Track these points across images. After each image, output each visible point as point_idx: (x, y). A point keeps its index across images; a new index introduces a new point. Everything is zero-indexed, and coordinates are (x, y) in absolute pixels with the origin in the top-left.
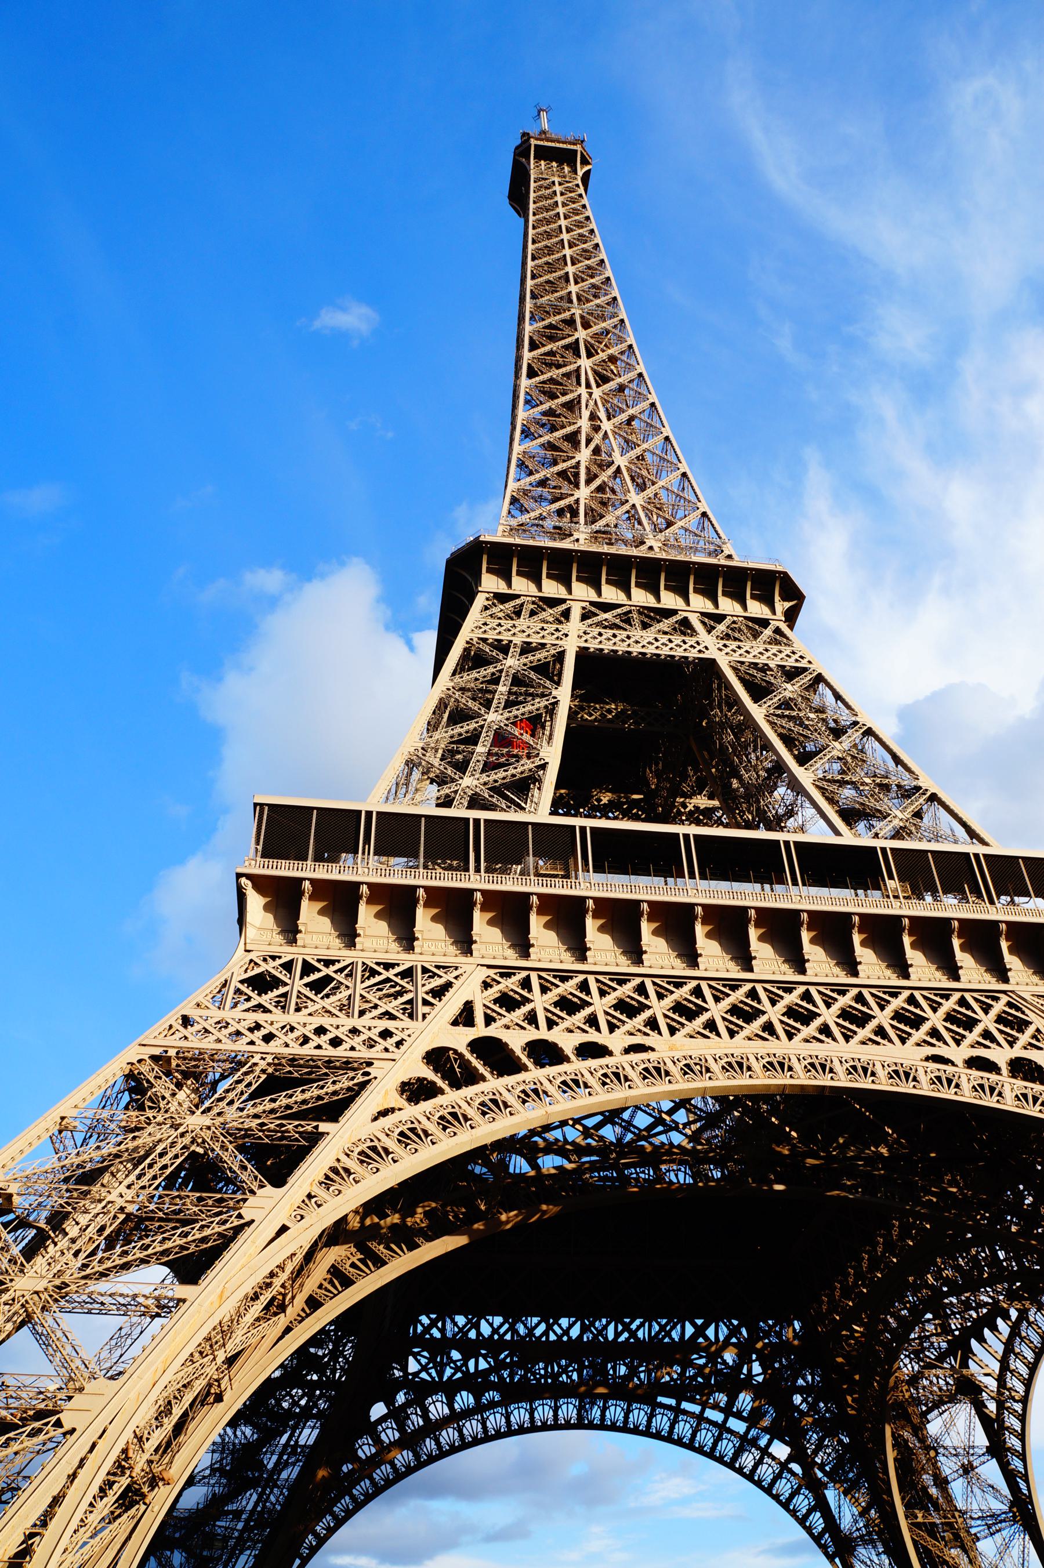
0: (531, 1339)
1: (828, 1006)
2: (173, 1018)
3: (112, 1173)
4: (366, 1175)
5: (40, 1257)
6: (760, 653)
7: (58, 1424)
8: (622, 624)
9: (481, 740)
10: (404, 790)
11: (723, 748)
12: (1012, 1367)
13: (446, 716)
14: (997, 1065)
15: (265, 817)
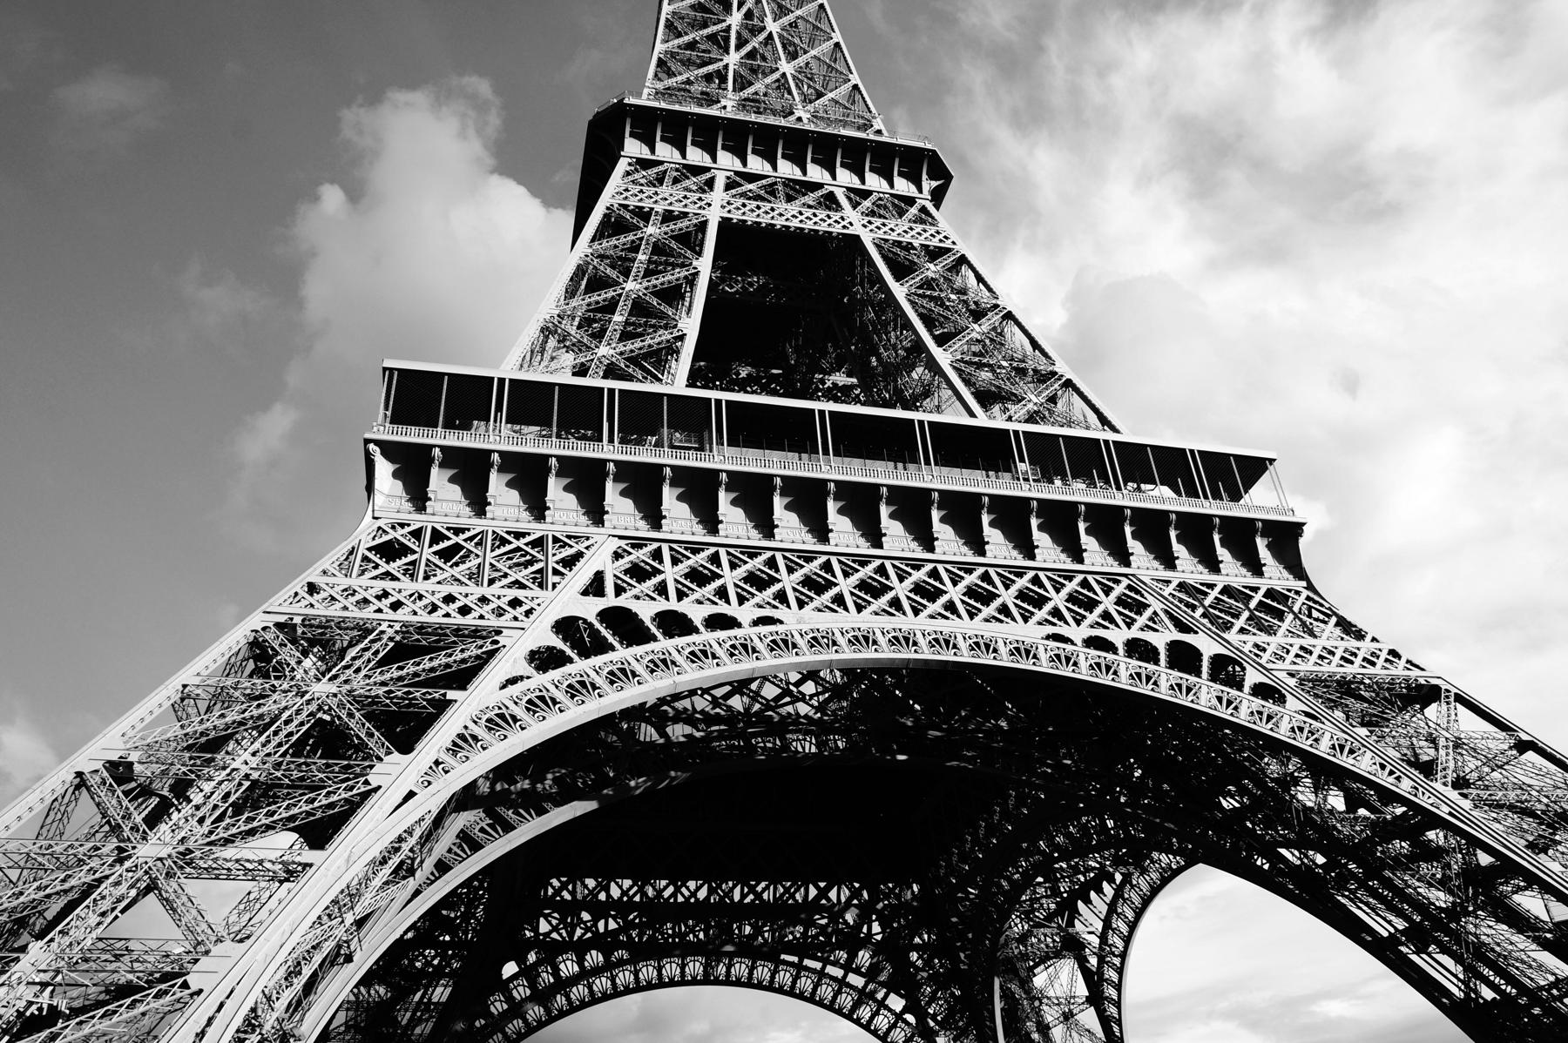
1: (955, 584)
2: (299, 585)
3: (237, 741)
4: (494, 742)
5: (164, 824)
6: (905, 232)
7: (185, 985)
8: (766, 196)
9: (619, 308)
10: (539, 358)
11: (864, 325)
12: (1114, 926)
13: (584, 283)
14: (736, 619)
15: (395, 382)
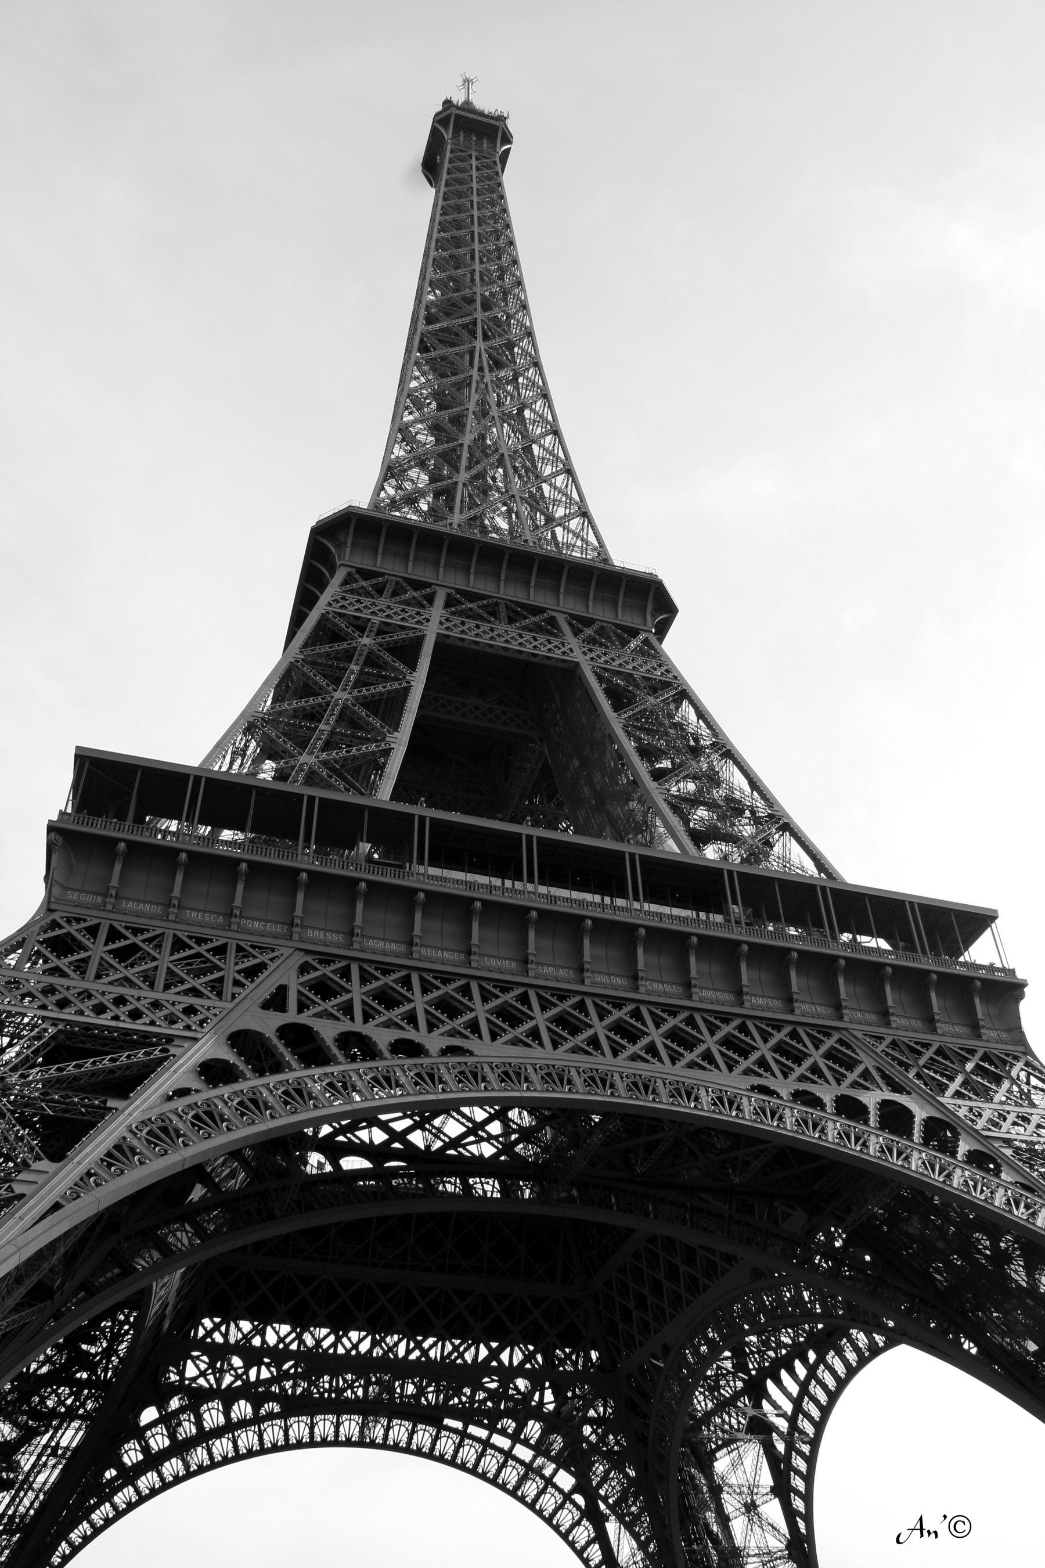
0: (317, 1350)
